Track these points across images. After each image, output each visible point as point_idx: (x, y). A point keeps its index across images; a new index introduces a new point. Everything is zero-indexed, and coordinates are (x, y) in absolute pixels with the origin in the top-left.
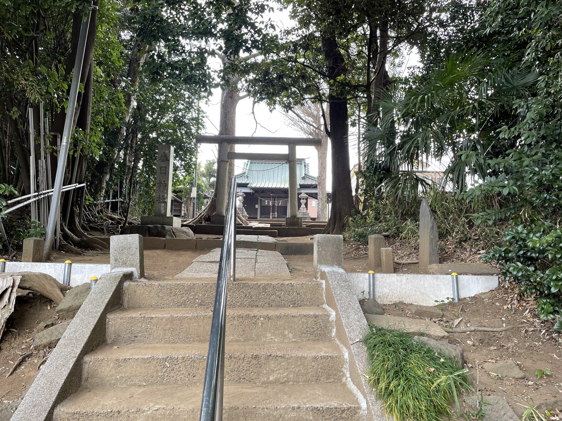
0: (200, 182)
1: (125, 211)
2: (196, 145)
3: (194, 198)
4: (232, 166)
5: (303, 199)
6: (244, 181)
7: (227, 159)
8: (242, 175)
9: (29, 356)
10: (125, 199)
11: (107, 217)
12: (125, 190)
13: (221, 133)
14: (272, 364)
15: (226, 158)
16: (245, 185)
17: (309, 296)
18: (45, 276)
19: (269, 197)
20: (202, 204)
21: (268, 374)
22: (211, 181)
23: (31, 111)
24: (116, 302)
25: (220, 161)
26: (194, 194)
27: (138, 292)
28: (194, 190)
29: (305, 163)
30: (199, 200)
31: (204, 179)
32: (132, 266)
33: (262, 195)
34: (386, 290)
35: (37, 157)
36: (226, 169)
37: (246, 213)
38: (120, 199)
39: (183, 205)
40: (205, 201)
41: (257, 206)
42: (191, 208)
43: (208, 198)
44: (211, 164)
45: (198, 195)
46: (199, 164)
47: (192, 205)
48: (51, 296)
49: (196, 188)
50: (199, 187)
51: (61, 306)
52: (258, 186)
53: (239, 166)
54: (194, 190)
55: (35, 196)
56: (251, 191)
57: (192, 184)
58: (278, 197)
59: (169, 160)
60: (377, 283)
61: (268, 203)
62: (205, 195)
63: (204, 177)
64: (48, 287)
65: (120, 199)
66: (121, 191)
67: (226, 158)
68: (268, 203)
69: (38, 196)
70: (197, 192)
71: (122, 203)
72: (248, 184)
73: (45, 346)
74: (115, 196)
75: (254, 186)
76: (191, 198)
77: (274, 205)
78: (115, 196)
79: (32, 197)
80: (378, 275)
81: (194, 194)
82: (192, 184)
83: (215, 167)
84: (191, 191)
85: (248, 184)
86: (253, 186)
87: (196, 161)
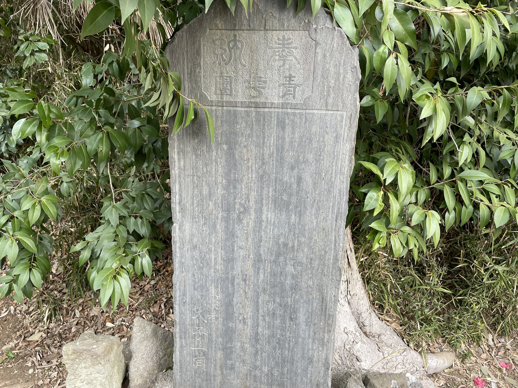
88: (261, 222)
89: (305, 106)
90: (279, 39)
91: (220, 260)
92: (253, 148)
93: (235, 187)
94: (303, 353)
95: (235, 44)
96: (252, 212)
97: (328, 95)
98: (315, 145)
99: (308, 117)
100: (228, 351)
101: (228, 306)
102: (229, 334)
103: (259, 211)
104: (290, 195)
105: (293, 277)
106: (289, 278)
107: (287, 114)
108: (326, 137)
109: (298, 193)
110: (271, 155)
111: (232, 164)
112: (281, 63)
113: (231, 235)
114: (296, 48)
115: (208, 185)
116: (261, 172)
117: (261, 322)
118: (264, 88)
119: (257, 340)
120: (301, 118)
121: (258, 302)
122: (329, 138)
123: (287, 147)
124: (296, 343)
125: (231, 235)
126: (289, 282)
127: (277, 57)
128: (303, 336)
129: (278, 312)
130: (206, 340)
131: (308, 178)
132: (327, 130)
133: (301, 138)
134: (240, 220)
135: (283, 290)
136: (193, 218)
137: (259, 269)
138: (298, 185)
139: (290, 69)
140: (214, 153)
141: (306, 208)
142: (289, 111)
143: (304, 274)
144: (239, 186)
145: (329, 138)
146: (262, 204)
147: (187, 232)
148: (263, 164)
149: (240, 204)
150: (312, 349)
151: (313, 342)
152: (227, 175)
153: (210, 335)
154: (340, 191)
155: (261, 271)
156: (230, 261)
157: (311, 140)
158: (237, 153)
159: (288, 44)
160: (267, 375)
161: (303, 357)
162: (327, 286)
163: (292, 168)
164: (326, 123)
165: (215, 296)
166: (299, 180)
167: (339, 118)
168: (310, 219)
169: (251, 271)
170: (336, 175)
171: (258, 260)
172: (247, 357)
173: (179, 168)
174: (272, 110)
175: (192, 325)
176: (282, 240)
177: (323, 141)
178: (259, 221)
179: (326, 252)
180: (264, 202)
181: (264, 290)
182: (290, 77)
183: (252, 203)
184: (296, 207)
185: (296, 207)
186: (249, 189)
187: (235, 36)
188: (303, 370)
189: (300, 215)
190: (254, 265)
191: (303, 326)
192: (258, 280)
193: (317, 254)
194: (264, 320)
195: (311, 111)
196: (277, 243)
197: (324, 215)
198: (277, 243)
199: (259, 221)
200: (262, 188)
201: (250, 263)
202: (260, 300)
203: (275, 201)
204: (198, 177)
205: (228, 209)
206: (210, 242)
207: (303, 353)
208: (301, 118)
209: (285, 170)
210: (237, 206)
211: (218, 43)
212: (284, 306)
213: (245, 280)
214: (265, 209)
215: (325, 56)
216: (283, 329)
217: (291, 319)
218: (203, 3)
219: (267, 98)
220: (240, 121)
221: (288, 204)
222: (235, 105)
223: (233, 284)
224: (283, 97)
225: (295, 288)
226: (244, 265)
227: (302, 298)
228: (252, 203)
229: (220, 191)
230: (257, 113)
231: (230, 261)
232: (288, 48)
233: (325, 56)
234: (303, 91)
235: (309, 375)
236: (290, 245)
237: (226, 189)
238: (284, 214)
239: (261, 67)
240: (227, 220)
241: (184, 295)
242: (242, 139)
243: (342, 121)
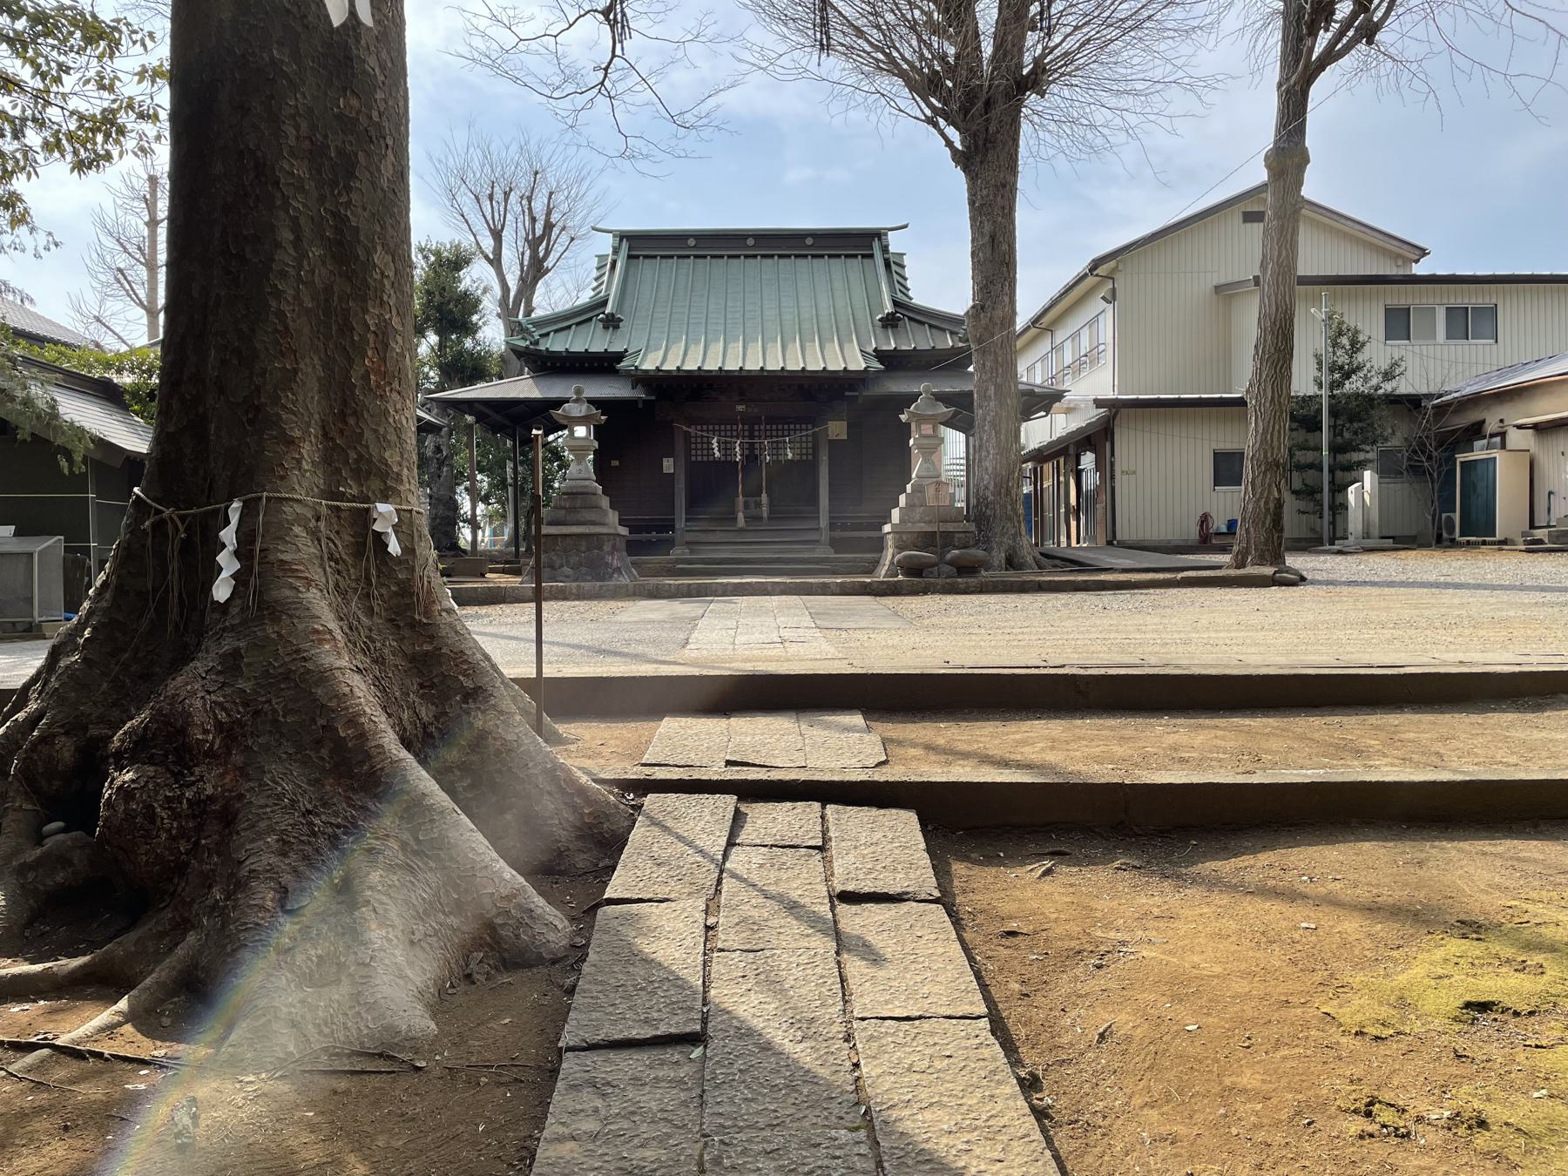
29: (885, 249)
58: (771, 420)
86: (649, 365)
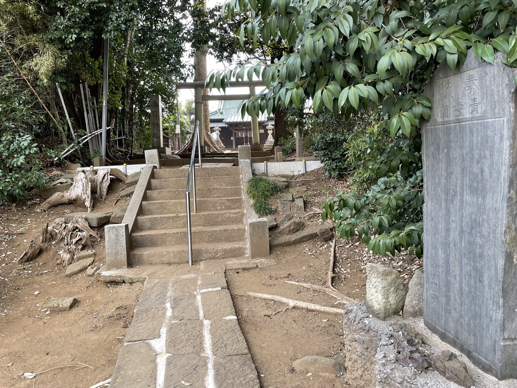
0: (182, 120)
1: (129, 145)
2: (176, 90)
3: (178, 134)
4: (206, 106)
5: (270, 130)
6: (219, 117)
7: (202, 101)
8: (216, 113)
9: (119, 200)
10: (127, 137)
11: (118, 150)
12: (127, 130)
13: (195, 80)
14: (215, 191)
15: (201, 100)
16: (220, 121)
17: (234, 172)
18: (119, 170)
19: (242, 130)
20: (185, 138)
21: (214, 195)
22: (191, 118)
23: (81, 85)
24: (153, 176)
25: (197, 102)
26: (178, 131)
27: (161, 173)
28: (178, 127)
30: (183, 136)
31: (185, 117)
32: (156, 163)
33: (236, 128)
34: (273, 170)
35: (88, 113)
36: (201, 109)
37: (223, 144)
38: (124, 137)
39: (170, 140)
40: (188, 136)
41: (232, 138)
42: (177, 143)
43: (190, 133)
44: (190, 103)
45: (182, 131)
46: (180, 103)
47: (177, 140)
48: (121, 178)
49: (179, 125)
50: (182, 124)
51: (126, 182)
52: (231, 121)
53: (213, 106)
54: (178, 127)
55: (90, 136)
56: (226, 126)
57: (175, 122)
59: (158, 106)
60: (268, 167)
61: (242, 134)
62: (187, 131)
63: (186, 115)
64: (120, 174)
65: (124, 137)
66: (124, 131)
67: (201, 100)
68: (242, 134)
69: (92, 135)
70: (181, 128)
71: (125, 140)
72: (223, 119)
73: (125, 196)
74: (120, 135)
75: (228, 120)
76: (176, 134)
77: (246, 137)
78: (120, 135)
79: (88, 137)
80: (269, 164)
81: (178, 131)
82: (175, 122)
83: (194, 105)
84: (175, 128)
85: (223, 119)
87: (177, 103)
88: (463, 202)
89: (483, 117)
90: (467, 77)
91: (443, 230)
92: (458, 150)
93: (450, 178)
94: (487, 312)
95: (449, 85)
96: (458, 195)
97: (495, 107)
98: (490, 144)
99: (485, 124)
100: (448, 297)
101: (447, 262)
102: (448, 284)
103: (462, 195)
104: (478, 183)
105: (481, 247)
106: (478, 247)
107: (474, 124)
108: (496, 137)
109: (481, 181)
110: (467, 154)
111: (449, 162)
112: (469, 91)
113: (448, 211)
114: (476, 80)
115: (438, 176)
116: (462, 166)
117: (464, 280)
118: (462, 109)
119: (462, 294)
120: (481, 126)
121: (461, 263)
122: (497, 139)
123: (475, 147)
124: (483, 302)
125: (448, 211)
126: (478, 251)
127: (467, 88)
128: (486, 296)
129: (472, 274)
130: (438, 287)
131: (486, 170)
132: (496, 132)
133: (482, 140)
134: (453, 201)
135: (475, 256)
136: (432, 199)
137: (462, 238)
138: (482, 175)
139: (474, 94)
140: (441, 155)
141: (487, 192)
142: (475, 122)
143: (486, 245)
144: (452, 177)
145: (497, 139)
146: (463, 190)
147: (429, 208)
148: (463, 160)
149: (453, 189)
150: (492, 310)
151: (493, 304)
152: (447, 169)
153: (439, 283)
154: (504, 178)
155: (463, 240)
156: (448, 230)
157: (487, 141)
158: (451, 154)
159: (472, 78)
160: (467, 324)
161: (486, 315)
162: (498, 256)
163: (478, 163)
164: (495, 127)
165: (441, 255)
166: (482, 171)
167: (502, 122)
168: (489, 201)
169: (458, 240)
170: (502, 166)
171: (462, 232)
172: (457, 306)
173: (426, 166)
174: (467, 123)
175: (431, 274)
176: (473, 217)
177: (494, 141)
178: (462, 202)
179: (496, 227)
180: (464, 188)
181: (465, 255)
182: (475, 99)
183: (458, 189)
184: (482, 192)
185: (482, 192)
186: (457, 178)
187: (448, 80)
188: (486, 326)
189: (484, 197)
190: (459, 234)
191: (487, 289)
192: (461, 246)
193: (492, 229)
194: (465, 278)
195: (487, 120)
196: (471, 219)
197: (496, 198)
198: (471, 219)
199: (462, 202)
200: (463, 178)
201: (457, 233)
202: (463, 262)
203: (470, 187)
204: (434, 171)
205: (447, 193)
206: (439, 217)
207: (487, 312)
208: (481, 126)
209: (474, 164)
210: (451, 191)
211: (441, 86)
212: (475, 269)
213: (455, 245)
214: (465, 193)
215: (491, 81)
216: (475, 288)
217: (480, 281)
218: (219, 379)
219: (463, 116)
220: (452, 133)
221: (477, 189)
222: (449, 122)
223: (449, 247)
224: (472, 113)
225: (481, 256)
226: (454, 235)
227: (486, 264)
228: (458, 189)
229: (443, 181)
230: (460, 126)
231: (448, 230)
232: (472, 81)
233: (491, 81)
234: (482, 107)
235: (490, 332)
236: (478, 221)
237: (446, 179)
238: (475, 196)
239: (460, 96)
240: (446, 200)
241: (428, 252)
242: (453, 145)
243: (504, 125)
